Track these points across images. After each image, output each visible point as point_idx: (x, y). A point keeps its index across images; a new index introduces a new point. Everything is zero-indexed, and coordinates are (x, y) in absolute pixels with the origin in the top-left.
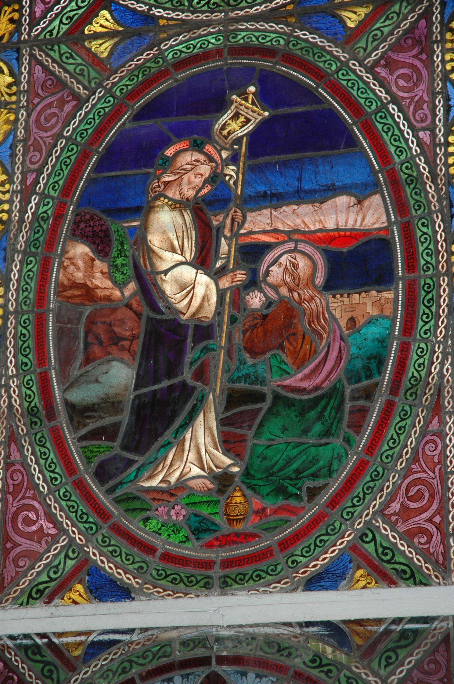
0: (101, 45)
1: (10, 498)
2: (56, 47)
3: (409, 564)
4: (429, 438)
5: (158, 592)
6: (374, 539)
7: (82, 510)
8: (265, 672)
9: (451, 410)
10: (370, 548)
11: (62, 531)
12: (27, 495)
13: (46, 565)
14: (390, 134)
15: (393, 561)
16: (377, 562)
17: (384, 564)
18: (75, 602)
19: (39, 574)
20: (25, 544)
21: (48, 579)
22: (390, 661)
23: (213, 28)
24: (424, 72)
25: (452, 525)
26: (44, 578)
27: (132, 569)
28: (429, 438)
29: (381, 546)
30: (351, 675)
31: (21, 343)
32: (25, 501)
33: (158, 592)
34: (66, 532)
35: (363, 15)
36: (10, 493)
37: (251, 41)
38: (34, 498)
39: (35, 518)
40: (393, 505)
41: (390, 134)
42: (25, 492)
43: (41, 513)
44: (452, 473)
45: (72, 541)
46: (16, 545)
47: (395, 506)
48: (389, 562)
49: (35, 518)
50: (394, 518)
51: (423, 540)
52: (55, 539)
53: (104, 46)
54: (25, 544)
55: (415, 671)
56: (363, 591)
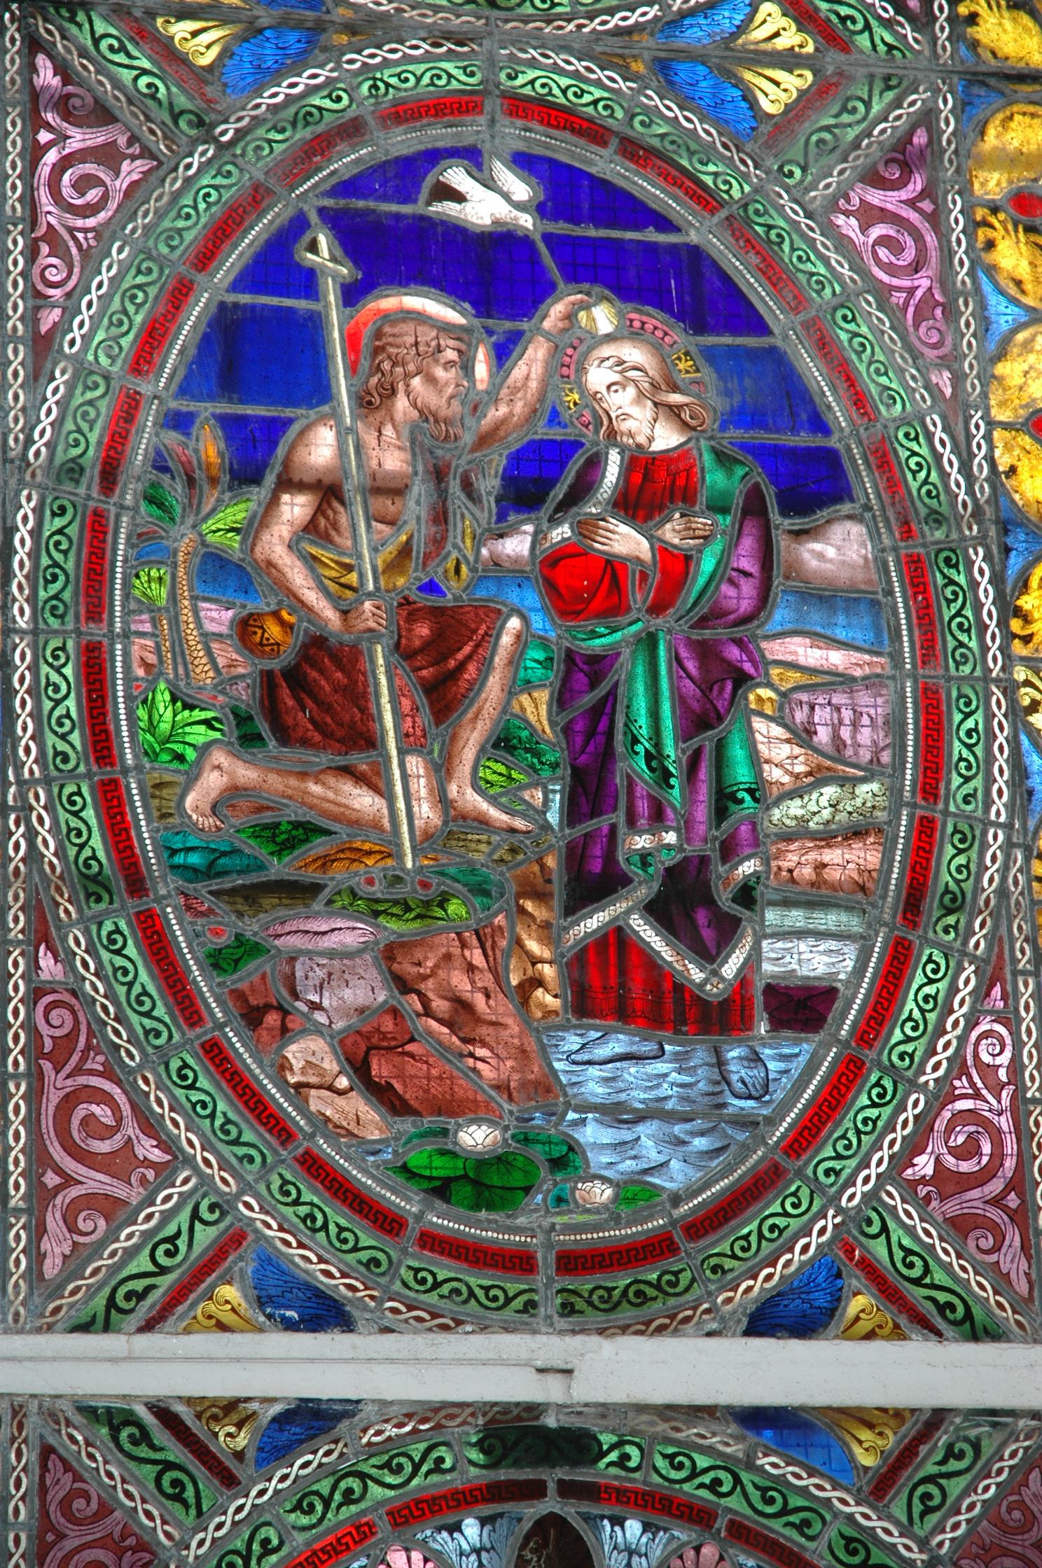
0: (195, 34)
1: (47, 1066)
2: (81, 17)
3: (960, 1291)
4: (984, 1027)
5: (419, 1319)
6: (885, 1229)
7: (224, 1114)
8: (662, 1520)
9: (1037, 1095)
10: (879, 1249)
11: (177, 1157)
12: (89, 1065)
13: (146, 1235)
14: (137, 990)
15: (927, 1280)
16: (892, 1277)
17: (906, 1284)
18: (222, 1327)
19: (131, 1253)
20: (95, 1181)
21: (151, 1268)
22: (931, 1504)
23: (781, 197)
24: (930, 239)
25: (1037, 1162)
26: (142, 1263)
27: (354, 1263)
28: (984, 1027)
29: (901, 1246)
30: (855, 1535)
31: (48, 705)
32: (82, 1080)
33: (419, 1319)
34: (189, 1161)
35: (795, 95)
36: (942, 304)
37: (550, 93)
38: (107, 1074)
39: (110, 1121)
40: (920, 1160)
41: (137, 990)
42: (84, 1059)
43: (126, 1109)
44: (1034, 1101)
45: (205, 1181)
46: (69, 1181)
47: (924, 1165)
48: (917, 1282)
49: (110, 1121)
50: (923, 1191)
51: (988, 1243)
52: (165, 1173)
53: (205, 38)
54: (95, 1181)
55: (985, 1523)
56: (867, 1345)
